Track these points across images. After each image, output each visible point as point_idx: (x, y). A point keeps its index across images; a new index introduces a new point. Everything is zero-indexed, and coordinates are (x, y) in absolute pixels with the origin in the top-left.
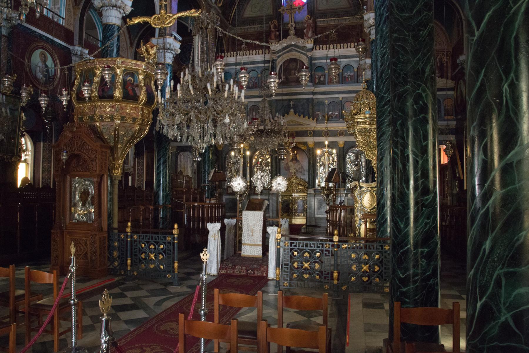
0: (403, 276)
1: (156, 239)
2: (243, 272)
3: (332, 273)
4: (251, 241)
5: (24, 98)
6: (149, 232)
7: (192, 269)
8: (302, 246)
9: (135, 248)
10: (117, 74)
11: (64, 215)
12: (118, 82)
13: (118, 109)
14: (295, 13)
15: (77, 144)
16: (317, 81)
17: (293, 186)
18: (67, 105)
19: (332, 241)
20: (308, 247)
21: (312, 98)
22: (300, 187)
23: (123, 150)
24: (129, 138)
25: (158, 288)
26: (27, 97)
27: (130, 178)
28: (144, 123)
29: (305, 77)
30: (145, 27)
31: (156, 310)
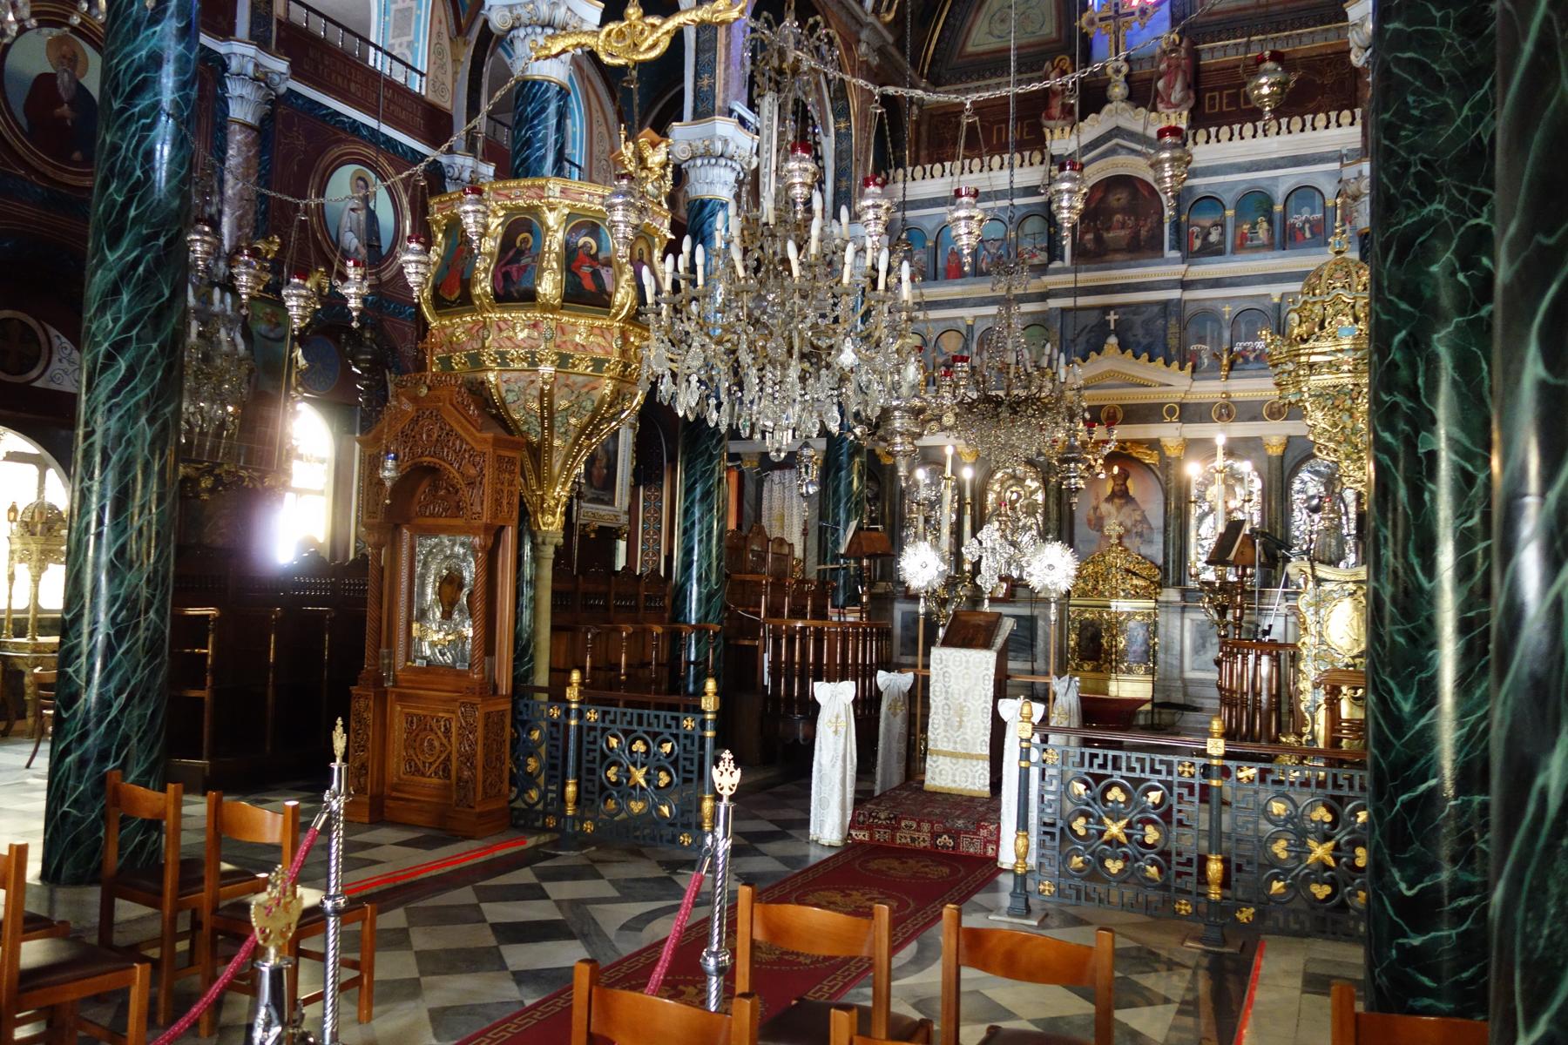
0: (1410, 888)
1: (649, 724)
2: (924, 839)
3: (1203, 861)
4: (955, 743)
5: (243, 290)
6: (649, 703)
7: (771, 821)
8: (1100, 766)
9: (589, 750)
10: (548, 229)
11: (390, 644)
12: (550, 252)
13: (549, 332)
14: (1130, 28)
15: (429, 436)
16: (1197, 243)
17: (1114, 576)
18: (362, 312)
19: (1203, 753)
20: (1120, 769)
21: (1180, 300)
22: (1135, 582)
23: (567, 456)
24: (586, 419)
25: (648, 875)
26: (251, 288)
27: (622, 545)
28: (631, 374)
29: (1070, 199)
30: (667, 98)
31: (618, 945)
